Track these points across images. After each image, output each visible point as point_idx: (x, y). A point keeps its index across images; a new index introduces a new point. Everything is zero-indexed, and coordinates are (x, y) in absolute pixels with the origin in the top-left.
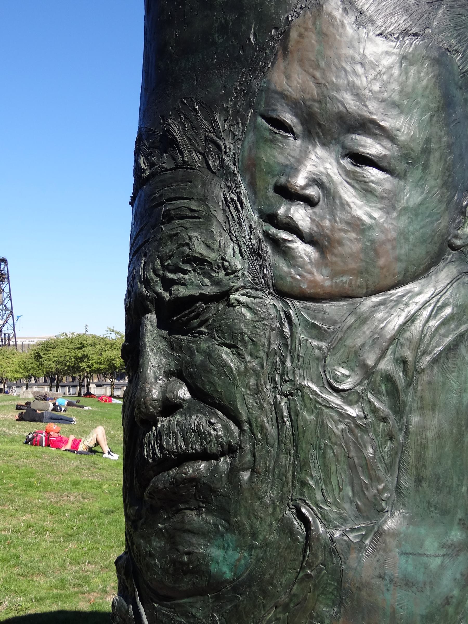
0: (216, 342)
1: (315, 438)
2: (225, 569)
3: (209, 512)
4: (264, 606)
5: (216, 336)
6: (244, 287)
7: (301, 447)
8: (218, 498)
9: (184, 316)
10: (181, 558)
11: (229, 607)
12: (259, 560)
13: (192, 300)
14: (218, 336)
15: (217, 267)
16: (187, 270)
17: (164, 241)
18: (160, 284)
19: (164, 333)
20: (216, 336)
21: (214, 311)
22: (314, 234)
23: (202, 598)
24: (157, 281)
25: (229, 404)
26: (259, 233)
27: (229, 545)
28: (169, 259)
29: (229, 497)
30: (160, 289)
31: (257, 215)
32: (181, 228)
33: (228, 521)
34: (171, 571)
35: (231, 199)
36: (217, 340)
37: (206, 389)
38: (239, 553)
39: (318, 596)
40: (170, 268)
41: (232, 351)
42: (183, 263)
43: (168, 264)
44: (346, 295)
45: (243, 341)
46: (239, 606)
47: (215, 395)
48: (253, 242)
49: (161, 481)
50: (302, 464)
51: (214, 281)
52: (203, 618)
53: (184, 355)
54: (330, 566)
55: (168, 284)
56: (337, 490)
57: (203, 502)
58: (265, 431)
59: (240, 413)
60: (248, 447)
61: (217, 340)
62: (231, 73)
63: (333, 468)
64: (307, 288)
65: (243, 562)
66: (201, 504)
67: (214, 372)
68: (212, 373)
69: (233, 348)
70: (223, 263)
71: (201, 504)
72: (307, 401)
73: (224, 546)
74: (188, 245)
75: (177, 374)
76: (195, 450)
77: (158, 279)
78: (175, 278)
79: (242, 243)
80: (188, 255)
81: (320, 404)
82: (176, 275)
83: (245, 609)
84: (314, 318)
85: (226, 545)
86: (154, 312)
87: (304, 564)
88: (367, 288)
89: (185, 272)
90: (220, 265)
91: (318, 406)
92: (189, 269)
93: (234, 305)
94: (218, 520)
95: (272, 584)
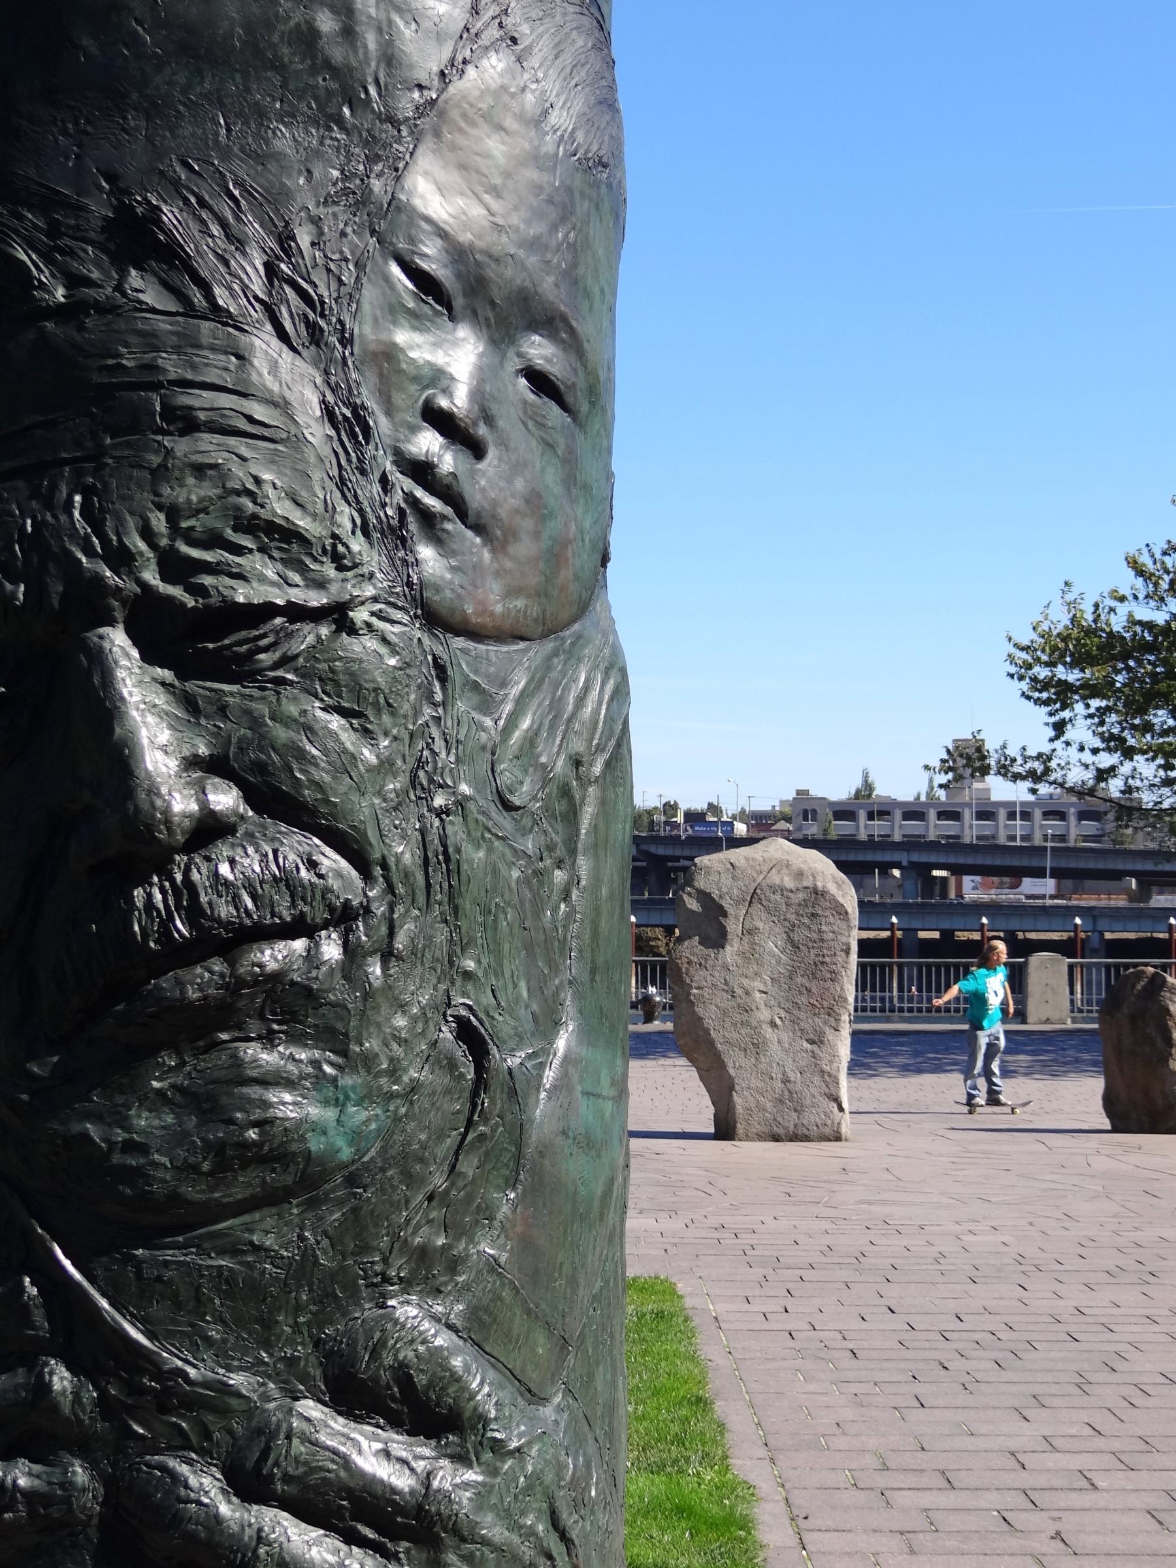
0: (317, 704)
1: (483, 894)
2: (340, 1142)
3: (296, 1039)
4: (407, 1202)
5: (319, 690)
6: (375, 599)
7: (464, 909)
8: (321, 1011)
9: (240, 643)
10: (241, 1134)
11: (337, 1216)
12: (400, 1120)
13: (268, 610)
14: (324, 692)
15: (320, 551)
16: (246, 548)
17: (177, 474)
18: (153, 566)
19: (160, 672)
20: (319, 690)
21: (311, 639)
22: (484, 513)
23: (273, 1210)
24: (148, 559)
25: (351, 827)
26: (398, 498)
27: (347, 1097)
28: (194, 516)
29: (344, 1007)
30: (150, 576)
31: (391, 458)
32: (227, 455)
33: (344, 1053)
34: (206, 1167)
35: (344, 415)
36: (322, 700)
37: (303, 796)
38: (366, 1109)
39: (489, 1172)
40: (195, 535)
41: (351, 724)
42: (235, 529)
43: (192, 528)
44: (519, 634)
45: (376, 704)
46: (361, 1208)
47: (323, 809)
48: (390, 512)
49: (192, 985)
50: (465, 942)
51: (313, 580)
52: (281, 1247)
53: (229, 724)
54: (509, 1117)
55: (175, 567)
56: (510, 986)
57: (279, 1023)
58: (412, 879)
59: (371, 844)
60: (380, 909)
61: (322, 700)
62: (322, 143)
63: (507, 947)
64: (474, 613)
65: (373, 1126)
66: (275, 1027)
67: (323, 765)
68: (317, 765)
69: (354, 718)
70: (334, 546)
71: (275, 1027)
72: (472, 825)
73: (337, 1100)
74: (251, 494)
75: (214, 766)
76: (280, 918)
77: (152, 555)
78: (209, 559)
79: (368, 510)
80: (255, 516)
81: (490, 831)
82: (211, 553)
83: (372, 1212)
84: (476, 672)
85: (341, 1097)
86: (121, 626)
87: (476, 1118)
88: (544, 624)
89: (238, 550)
90: (329, 548)
91: (487, 835)
92: (250, 546)
93: (361, 632)
94: (317, 1054)
95: (422, 1160)
